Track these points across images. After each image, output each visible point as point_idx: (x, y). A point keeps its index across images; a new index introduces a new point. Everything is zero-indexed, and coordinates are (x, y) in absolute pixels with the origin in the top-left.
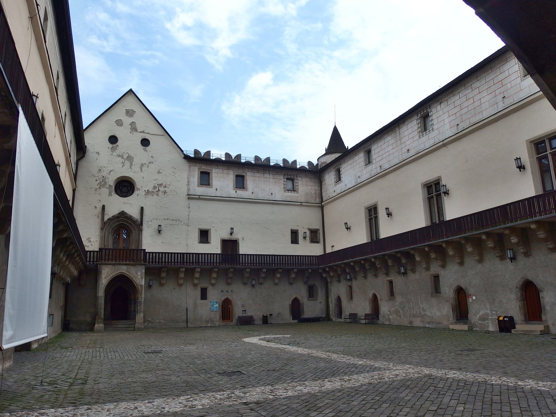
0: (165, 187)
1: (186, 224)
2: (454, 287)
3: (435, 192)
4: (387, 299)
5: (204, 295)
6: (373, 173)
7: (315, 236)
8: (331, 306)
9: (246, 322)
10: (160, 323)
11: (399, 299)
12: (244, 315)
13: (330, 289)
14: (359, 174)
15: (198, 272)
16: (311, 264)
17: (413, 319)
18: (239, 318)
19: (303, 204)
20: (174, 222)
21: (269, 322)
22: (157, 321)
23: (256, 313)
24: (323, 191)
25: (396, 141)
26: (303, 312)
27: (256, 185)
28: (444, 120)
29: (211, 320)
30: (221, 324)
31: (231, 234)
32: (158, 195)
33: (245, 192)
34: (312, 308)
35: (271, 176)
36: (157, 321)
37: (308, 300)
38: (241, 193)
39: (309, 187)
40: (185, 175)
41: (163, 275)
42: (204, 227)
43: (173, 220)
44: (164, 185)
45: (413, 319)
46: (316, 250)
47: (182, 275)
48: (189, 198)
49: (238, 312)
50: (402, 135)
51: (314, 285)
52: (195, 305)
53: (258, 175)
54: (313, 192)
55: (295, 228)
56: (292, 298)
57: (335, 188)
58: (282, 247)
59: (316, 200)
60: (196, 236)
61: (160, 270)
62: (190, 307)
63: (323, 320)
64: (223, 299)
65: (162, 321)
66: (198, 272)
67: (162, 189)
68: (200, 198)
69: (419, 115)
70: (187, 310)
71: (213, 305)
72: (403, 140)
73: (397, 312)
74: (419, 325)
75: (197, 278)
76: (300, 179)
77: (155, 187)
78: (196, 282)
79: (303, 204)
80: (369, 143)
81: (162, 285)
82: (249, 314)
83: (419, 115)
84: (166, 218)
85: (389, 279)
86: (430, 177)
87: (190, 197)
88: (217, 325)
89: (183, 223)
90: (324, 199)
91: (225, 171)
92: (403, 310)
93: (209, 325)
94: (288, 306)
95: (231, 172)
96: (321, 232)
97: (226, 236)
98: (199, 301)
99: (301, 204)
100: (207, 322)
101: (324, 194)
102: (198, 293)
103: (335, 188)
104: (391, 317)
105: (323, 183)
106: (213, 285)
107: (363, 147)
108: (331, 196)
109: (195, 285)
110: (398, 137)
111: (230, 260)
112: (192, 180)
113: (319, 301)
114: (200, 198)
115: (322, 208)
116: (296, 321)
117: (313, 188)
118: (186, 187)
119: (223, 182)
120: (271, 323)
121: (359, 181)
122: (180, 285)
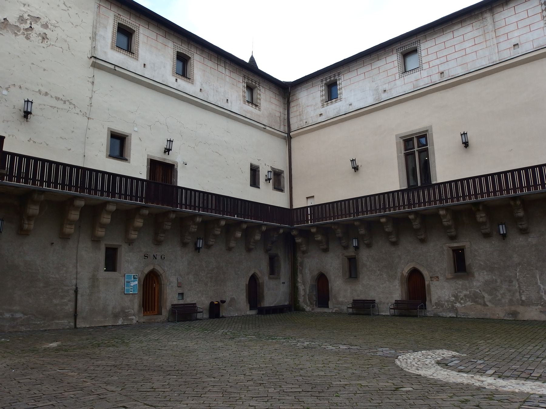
0: (45, 26)
1: (85, 115)
2: (316, 273)
3: (416, 150)
4: (449, 276)
5: (111, 262)
6: (422, 84)
7: (277, 179)
8: (301, 287)
9: (184, 314)
10: (13, 319)
11: (480, 278)
12: (181, 302)
13: (302, 264)
14: (386, 87)
15: (109, 212)
16: (441, 200)
17: (520, 309)
18: (174, 306)
19: (267, 128)
20: (60, 104)
21: (221, 315)
22: (7, 315)
23: (200, 299)
24: (291, 115)
25: (484, 34)
26: (263, 297)
27: (205, 78)
28: (435, 57)
29: (124, 313)
30: (142, 320)
31: (167, 150)
32: (28, 38)
33: (190, 85)
34: (275, 293)
35: (228, 72)
36: (7, 315)
37: (270, 278)
38: (182, 84)
39: (273, 107)
40: (89, 18)
41: (34, 210)
42: (120, 128)
43: (57, 99)
44: (44, 20)
45: (520, 309)
46: (278, 200)
47: (75, 215)
48: (95, 65)
49: (171, 297)
50: (498, 25)
51: (277, 255)
52: (94, 279)
53: (209, 63)
54: (278, 114)
55: (256, 163)
56: (250, 275)
57: (322, 111)
58: (238, 188)
59: (280, 128)
60: (102, 142)
61: (26, 197)
62: (84, 286)
63: (291, 308)
64: (147, 270)
65: (18, 315)
66: (109, 212)
67: (37, 27)
68: (115, 71)
69: (324, 82)
70: (76, 291)
71: (128, 282)
72: (501, 31)
73: (475, 298)
74: (536, 318)
75: (103, 226)
76: (263, 90)
77: (22, 19)
78: (100, 232)
79: (267, 128)
80: (413, 40)
81: (22, 232)
82: (188, 300)
83: (324, 82)
84: (44, 90)
85: (455, 245)
86: (412, 126)
87: (97, 64)
88: (134, 322)
89: (78, 111)
90: (293, 128)
91: (161, 39)
92: (490, 294)
93: (120, 322)
94: (245, 288)
95: (170, 44)
96: (286, 175)
97: (159, 155)
98: (102, 274)
99: (264, 128)
100: (116, 316)
101: (292, 121)
102: (101, 256)
103: (322, 111)
104: (458, 305)
105: (292, 104)
106: (130, 242)
107: (398, 46)
108: (310, 122)
109: (96, 240)
110: (490, 27)
111: (159, 202)
112: (101, 32)
113: (282, 280)
114: (115, 71)
115: (288, 139)
116: (254, 312)
117: (278, 109)
118: (89, 42)
119: (154, 57)
120: (223, 317)
121: (384, 96)
122: (65, 237)
